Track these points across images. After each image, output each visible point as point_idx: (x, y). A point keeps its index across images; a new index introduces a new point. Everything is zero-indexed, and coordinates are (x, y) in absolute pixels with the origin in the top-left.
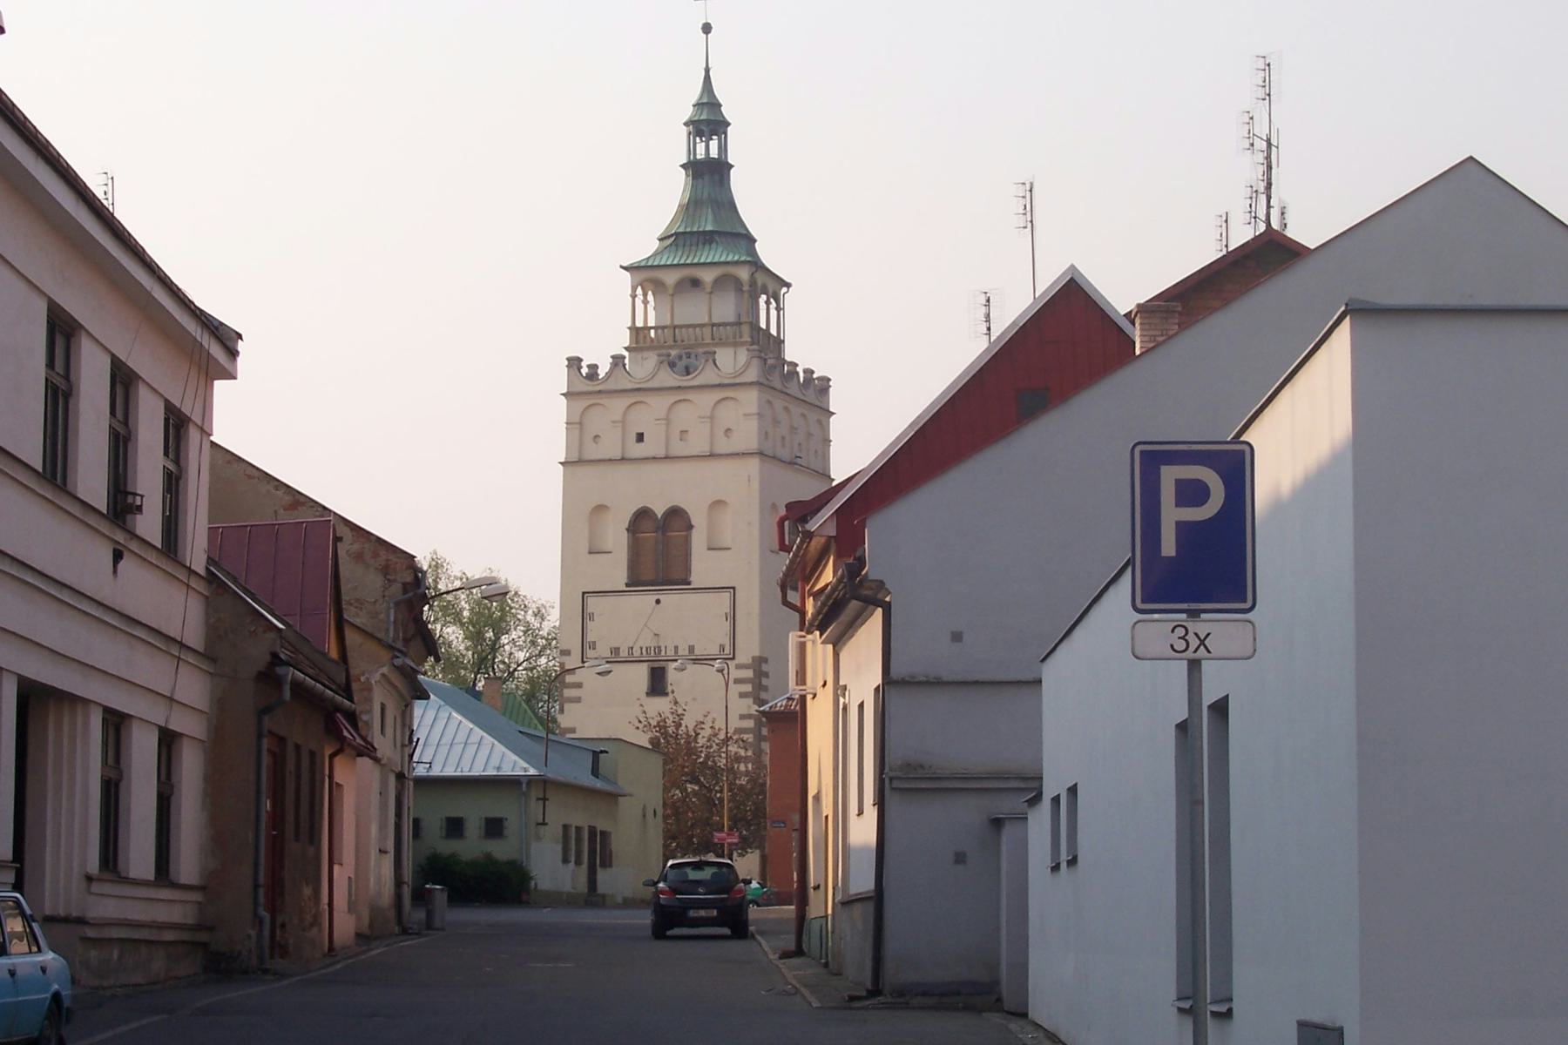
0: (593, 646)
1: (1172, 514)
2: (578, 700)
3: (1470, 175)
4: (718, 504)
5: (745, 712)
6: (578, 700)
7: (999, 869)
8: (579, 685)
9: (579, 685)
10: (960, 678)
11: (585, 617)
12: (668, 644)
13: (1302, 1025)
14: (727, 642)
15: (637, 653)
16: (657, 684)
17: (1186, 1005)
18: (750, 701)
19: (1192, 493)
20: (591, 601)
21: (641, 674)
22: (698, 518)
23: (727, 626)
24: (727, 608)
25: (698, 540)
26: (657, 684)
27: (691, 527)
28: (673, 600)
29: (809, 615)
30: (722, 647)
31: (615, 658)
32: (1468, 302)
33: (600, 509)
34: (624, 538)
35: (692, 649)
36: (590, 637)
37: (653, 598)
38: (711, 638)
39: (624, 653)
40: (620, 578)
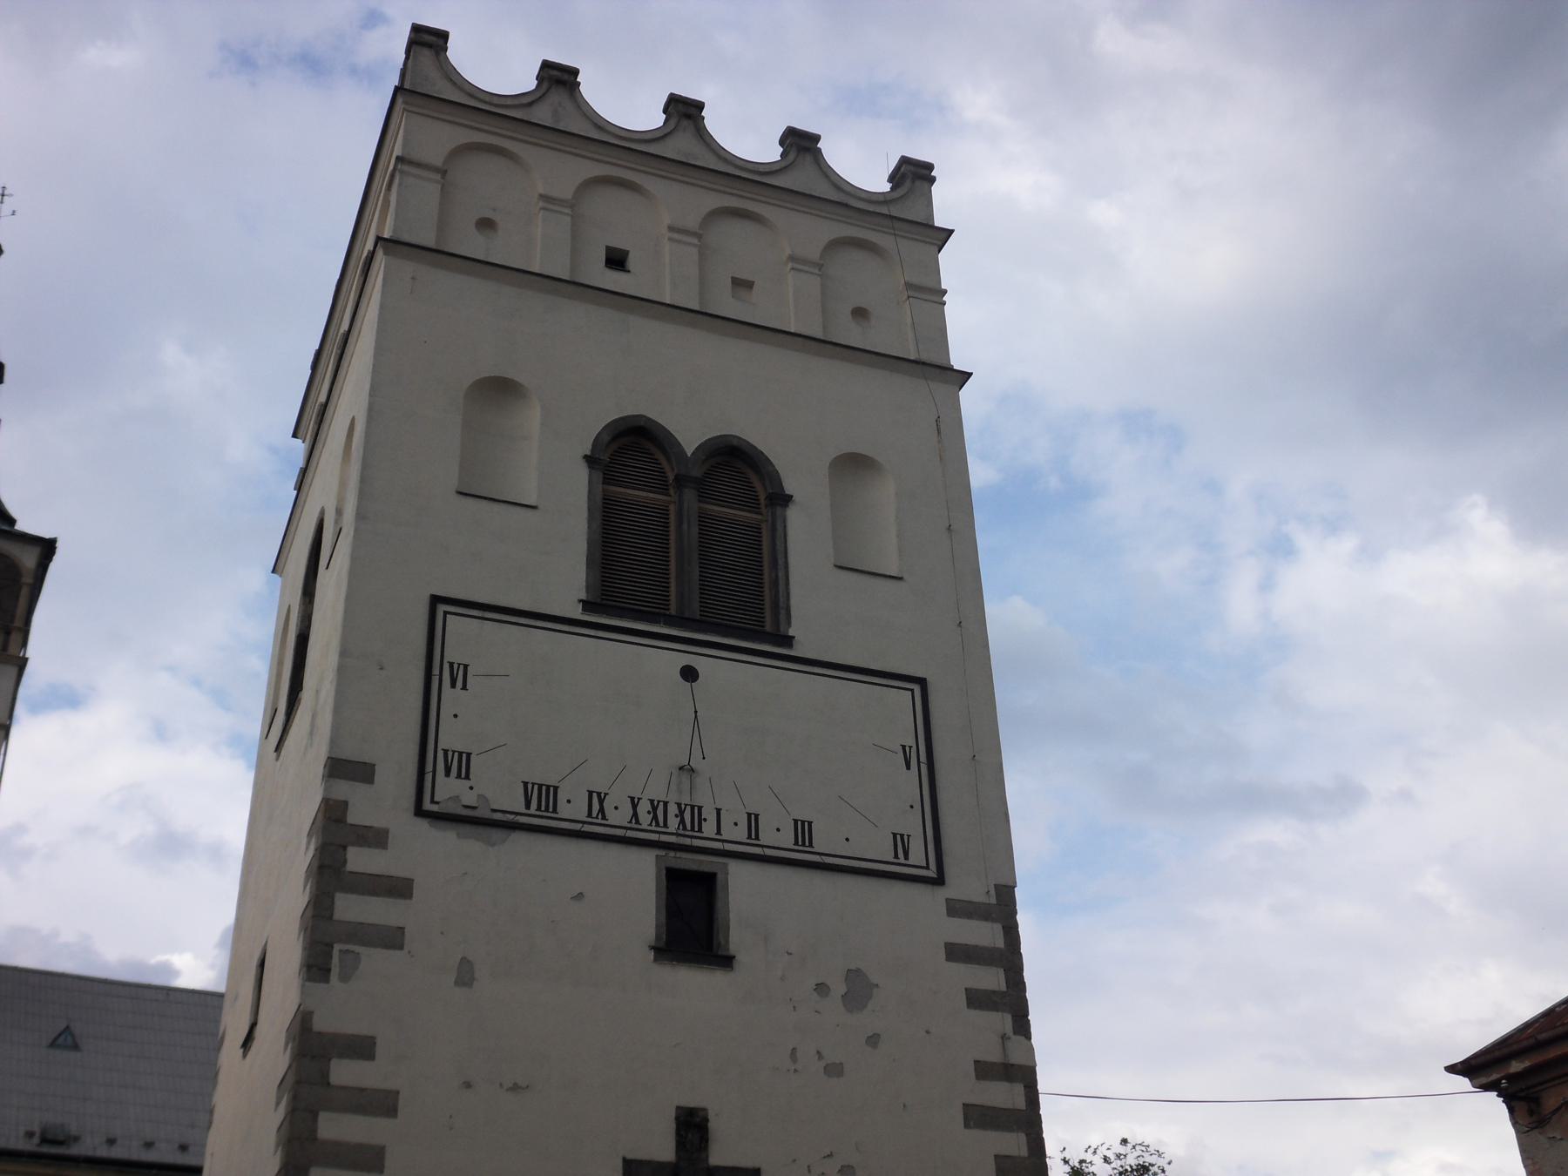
0: (461, 765)
2: (392, 939)
4: (853, 466)
6: (392, 939)
9: (400, 888)
10: (893, 882)
11: (437, 673)
12: (727, 803)
13: (996, 1157)
14: (912, 826)
16: (692, 925)
21: (632, 886)
22: (803, 478)
23: (909, 784)
24: (904, 731)
25: (806, 538)
26: (692, 925)
27: (781, 499)
28: (729, 677)
30: (900, 842)
31: (539, 816)
32: (416, 759)
33: (498, 391)
34: (578, 481)
36: (450, 737)
37: (665, 662)
39: (573, 808)
40: (564, 581)
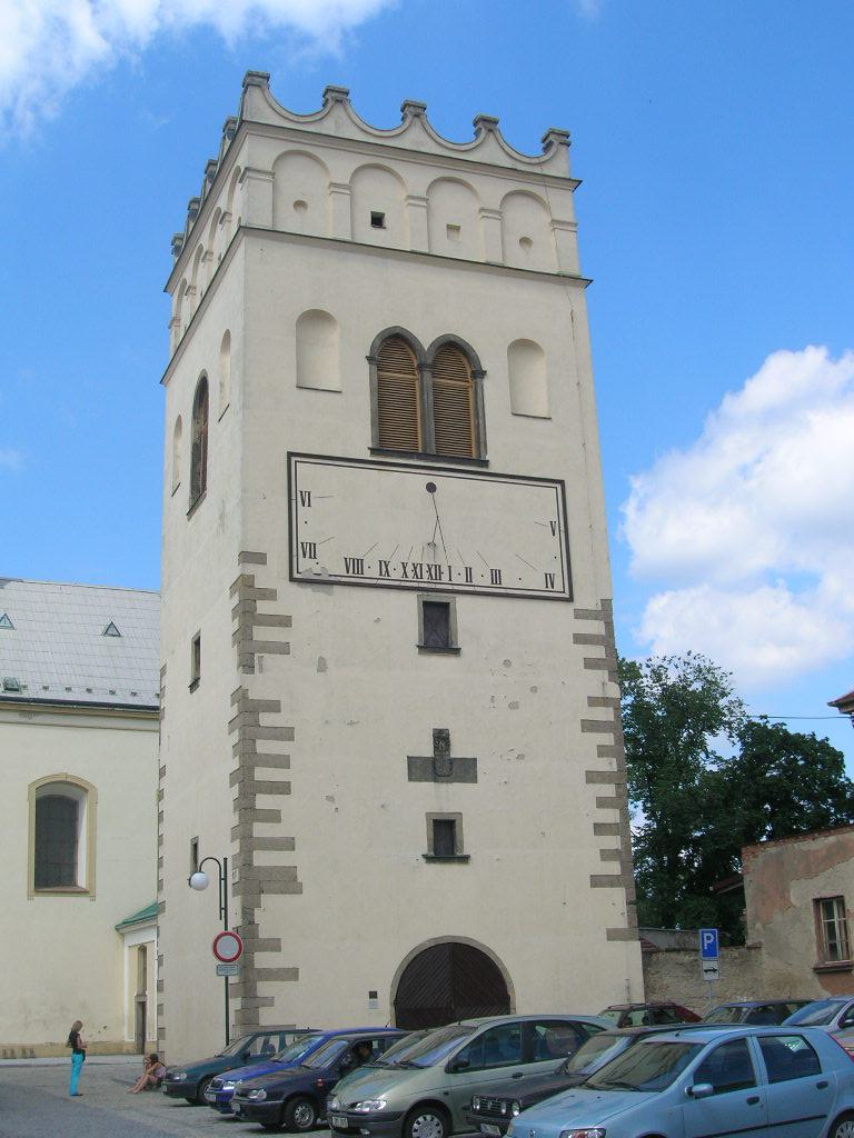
1: (706, 942)
2: (284, 649)
3: (841, 755)
4: (523, 347)
5: (598, 694)
6: (284, 649)
7: (670, 1085)
8: (284, 622)
11: (295, 498)
14: (556, 569)
15: (396, 574)
16: (437, 631)
17: (9, 1052)
18: (603, 674)
19: (709, 938)
20: (304, 470)
21: (405, 612)
22: (491, 357)
23: (554, 544)
25: (494, 394)
26: (437, 631)
27: (479, 374)
29: (565, 1059)
30: (549, 578)
34: (362, 376)
35: (496, 576)
36: (304, 536)
37: (422, 479)
38: (531, 564)
39: (371, 571)
40: (360, 440)
